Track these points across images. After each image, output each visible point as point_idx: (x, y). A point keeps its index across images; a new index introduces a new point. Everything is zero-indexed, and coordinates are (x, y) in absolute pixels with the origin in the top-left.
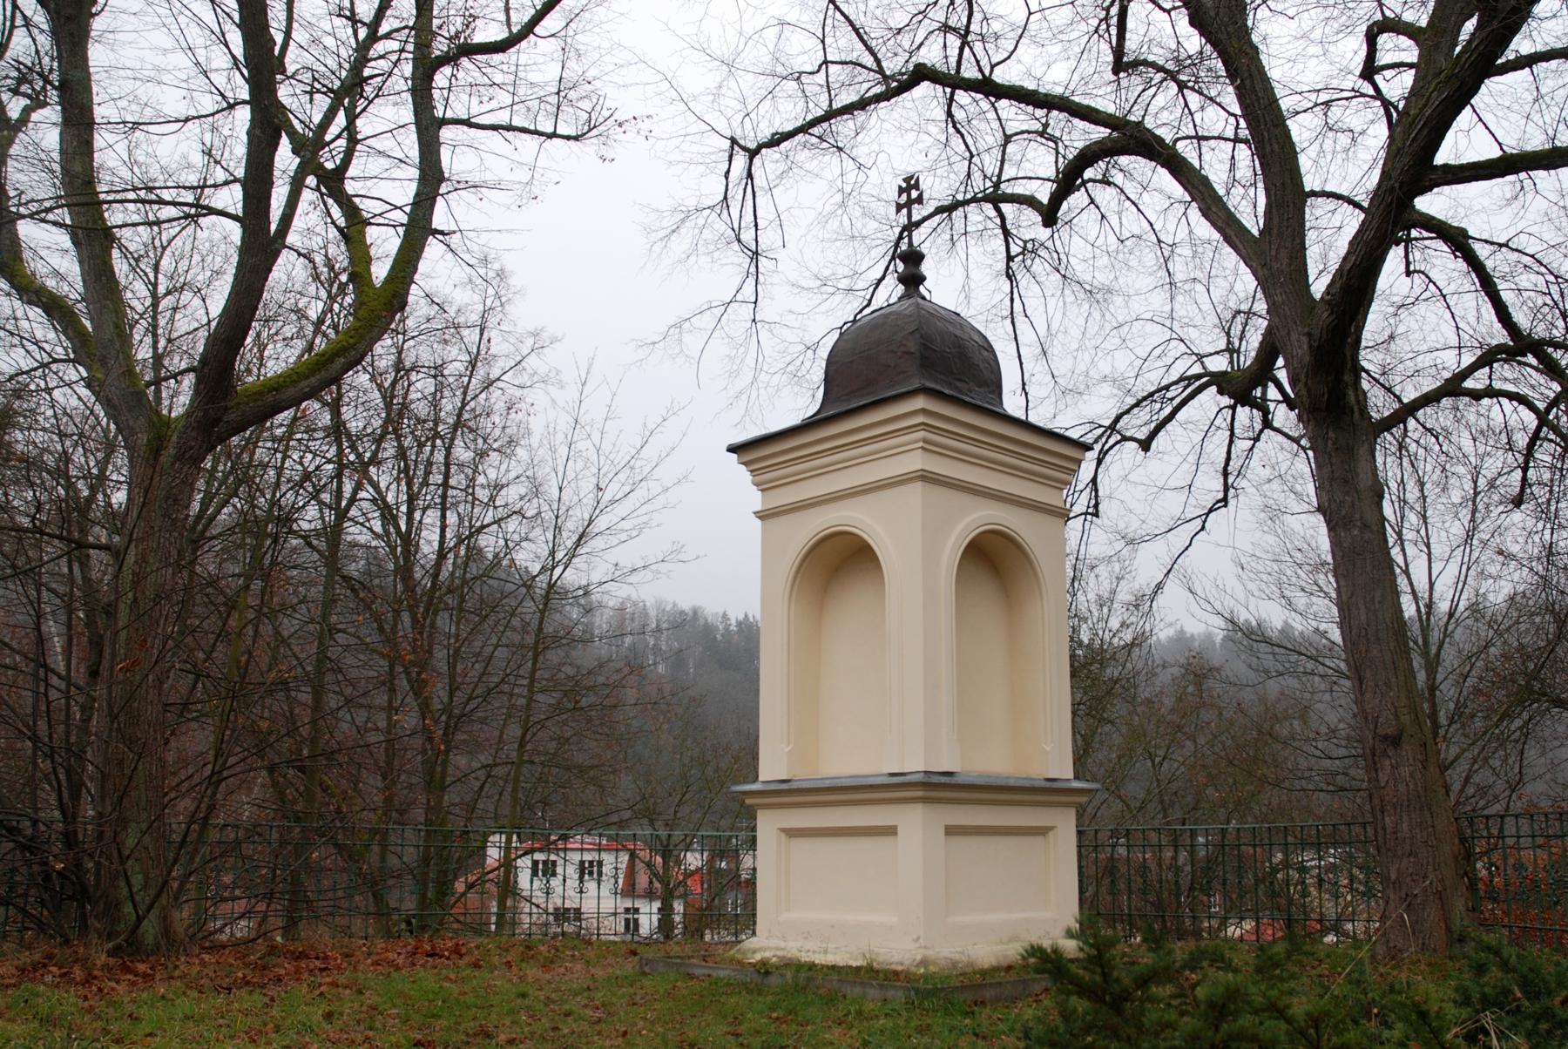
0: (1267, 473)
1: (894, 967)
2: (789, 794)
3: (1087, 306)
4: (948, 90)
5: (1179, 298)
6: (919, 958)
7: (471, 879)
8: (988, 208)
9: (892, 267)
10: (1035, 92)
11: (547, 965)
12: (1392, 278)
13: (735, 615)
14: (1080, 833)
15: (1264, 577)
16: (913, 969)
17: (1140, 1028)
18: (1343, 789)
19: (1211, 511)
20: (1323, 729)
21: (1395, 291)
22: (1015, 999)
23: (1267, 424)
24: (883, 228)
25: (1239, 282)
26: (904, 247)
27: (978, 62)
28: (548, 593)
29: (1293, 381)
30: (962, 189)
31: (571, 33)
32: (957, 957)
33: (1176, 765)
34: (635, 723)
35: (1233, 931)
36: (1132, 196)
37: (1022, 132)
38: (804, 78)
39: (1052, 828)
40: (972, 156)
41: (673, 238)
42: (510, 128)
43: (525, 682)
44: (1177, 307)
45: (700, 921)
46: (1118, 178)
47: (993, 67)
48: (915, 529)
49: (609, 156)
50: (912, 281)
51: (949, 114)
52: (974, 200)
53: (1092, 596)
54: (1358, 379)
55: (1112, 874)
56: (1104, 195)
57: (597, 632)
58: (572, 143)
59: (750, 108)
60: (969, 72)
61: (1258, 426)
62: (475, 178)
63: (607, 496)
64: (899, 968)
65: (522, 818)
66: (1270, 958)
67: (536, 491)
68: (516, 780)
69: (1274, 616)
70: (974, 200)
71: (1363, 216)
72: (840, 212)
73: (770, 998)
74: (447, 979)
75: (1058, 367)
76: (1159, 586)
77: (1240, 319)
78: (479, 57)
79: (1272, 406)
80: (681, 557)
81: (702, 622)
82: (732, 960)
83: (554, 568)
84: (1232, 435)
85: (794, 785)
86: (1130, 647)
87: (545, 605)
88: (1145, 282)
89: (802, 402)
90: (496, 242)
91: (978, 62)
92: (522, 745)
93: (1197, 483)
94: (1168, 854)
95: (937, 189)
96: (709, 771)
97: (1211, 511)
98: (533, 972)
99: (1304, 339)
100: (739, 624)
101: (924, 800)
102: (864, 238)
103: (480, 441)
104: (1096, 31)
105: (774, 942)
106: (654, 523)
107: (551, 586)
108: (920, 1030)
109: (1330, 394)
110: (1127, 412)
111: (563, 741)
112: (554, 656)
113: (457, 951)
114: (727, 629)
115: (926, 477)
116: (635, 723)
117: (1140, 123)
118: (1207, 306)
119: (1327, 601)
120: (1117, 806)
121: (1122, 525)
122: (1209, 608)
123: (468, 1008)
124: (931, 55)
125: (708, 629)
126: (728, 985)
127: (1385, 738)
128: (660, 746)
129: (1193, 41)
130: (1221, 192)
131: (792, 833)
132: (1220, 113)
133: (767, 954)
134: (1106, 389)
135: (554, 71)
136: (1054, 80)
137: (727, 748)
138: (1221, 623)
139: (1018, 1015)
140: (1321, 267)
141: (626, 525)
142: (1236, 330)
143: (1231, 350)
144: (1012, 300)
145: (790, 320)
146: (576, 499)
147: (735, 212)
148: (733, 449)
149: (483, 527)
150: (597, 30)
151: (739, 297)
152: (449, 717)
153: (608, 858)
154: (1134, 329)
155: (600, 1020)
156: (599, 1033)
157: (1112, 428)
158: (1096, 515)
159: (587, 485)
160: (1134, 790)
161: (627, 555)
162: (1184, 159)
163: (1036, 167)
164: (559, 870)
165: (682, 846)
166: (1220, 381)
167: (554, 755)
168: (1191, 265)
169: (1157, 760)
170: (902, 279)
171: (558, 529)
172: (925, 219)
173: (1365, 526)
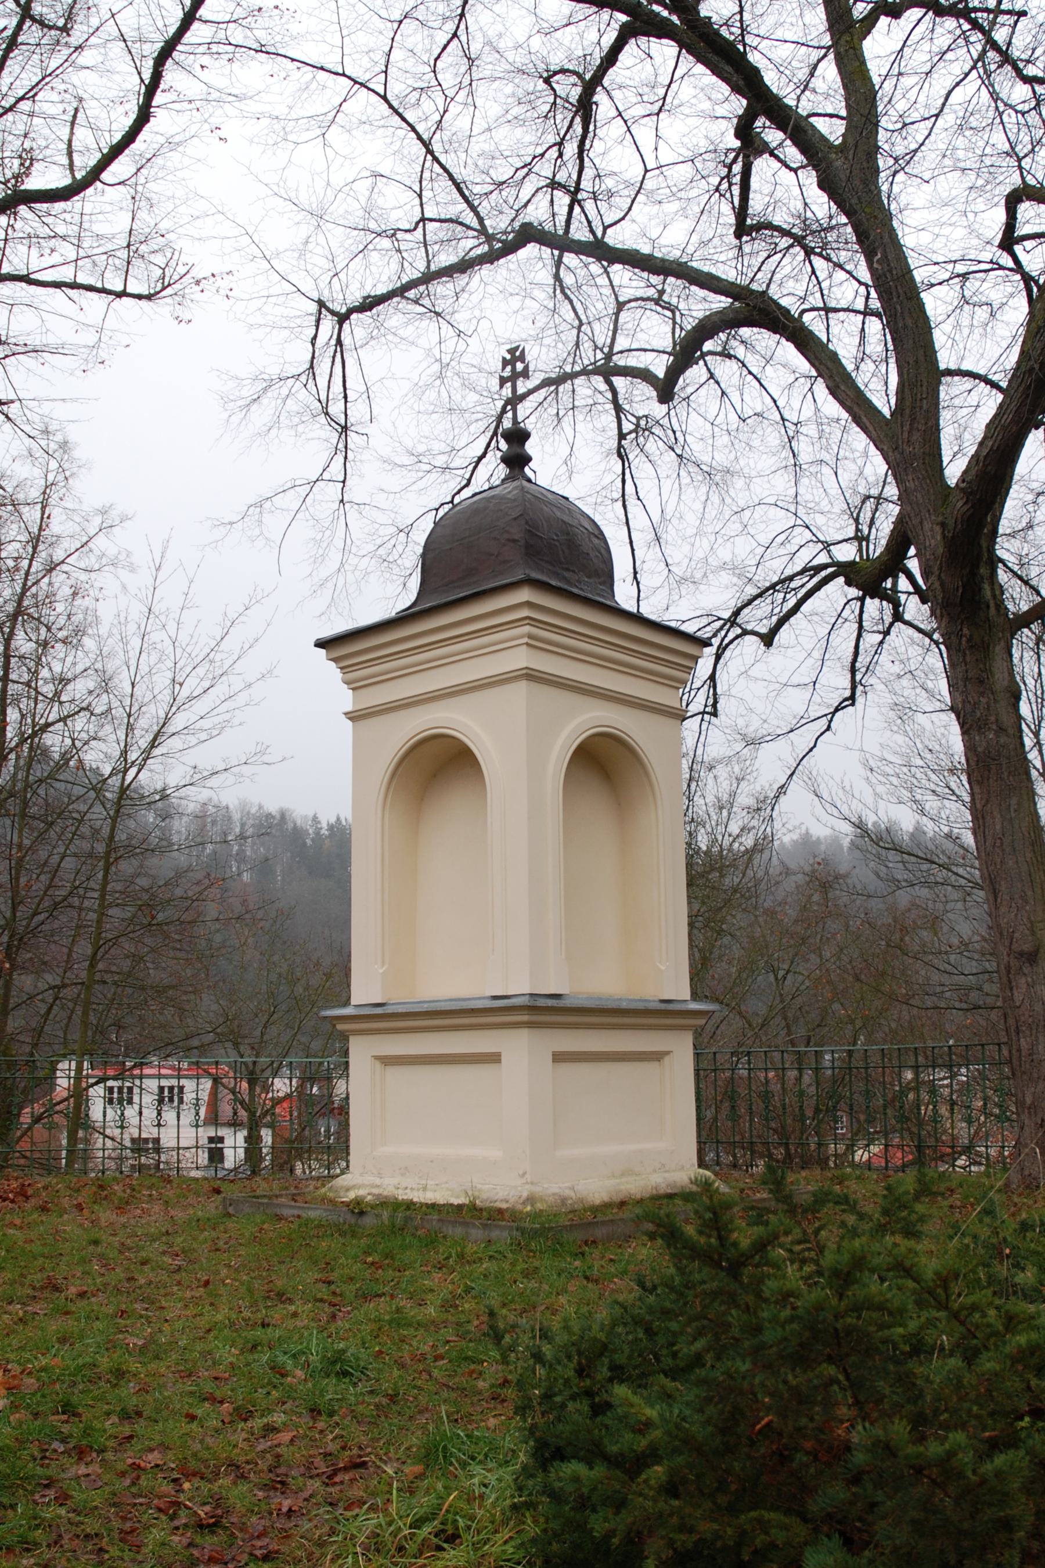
0: (897, 668)
1: (498, 1205)
2: (383, 1019)
3: (704, 489)
4: (556, 252)
5: (804, 481)
6: (525, 1194)
7: (38, 1109)
8: (599, 381)
9: (493, 444)
10: (650, 257)
11: (121, 1208)
12: (1032, 462)
13: (327, 818)
14: (697, 1055)
15: (895, 780)
16: (519, 1207)
17: (759, 1295)
18: (977, 1007)
19: (837, 710)
20: (955, 941)
21: (1034, 477)
22: (628, 1238)
23: (898, 617)
24: (484, 403)
25: (868, 465)
26: (507, 424)
27: (589, 222)
28: (120, 798)
29: (925, 575)
30: (570, 360)
31: (142, 180)
32: (568, 1193)
33: (801, 978)
34: (218, 938)
35: (860, 1155)
36: (754, 371)
37: (636, 300)
38: (400, 235)
39: (668, 1053)
40: (581, 324)
41: (254, 407)
42: (74, 286)
43: (96, 895)
44: (801, 490)
45: (290, 1150)
46: (740, 351)
47: (605, 228)
48: (517, 730)
49: (186, 317)
50: (517, 461)
51: (557, 277)
52: (584, 372)
53: (710, 799)
54: (994, 574)
55: (731, 1098)
56: (726, 370)
57: (175, 839)
58: (143, 303)
59: (339, 267)
60: (579, 233)
61: (888, 619)
62: (35, 341)
63: (185, 692)
64: (504, 1206)
65: (94, 1042)
66: (897, 1200)
67: (105, 685)
68: (87, 1003)
69: (905, 820)
70: (584, 372)
71: (1000, 397)
72: (438, 382)
73: (364, 1241)
74: (12, 1225)
75: (675, 554)
76: (782, 790)
77: (869, 505)
78: (37, 206)
79: (903, 598)
80: (266, 758)
81: (290, 826)
82: (323, 1199)
83: (126, 771)
84: (861, 627)
85: (389, 1010)
86: (751, 853)
87: (117, 811)
88: (767, 463)
89: (394, 590)
90: (60, 412)
91: (589, 222)
92: (92, 966)
93: (822, 680)
94: (792, 1074)
95: (543, 360)
96: (299, 990)
97: (837, 710)
98: (106, 1215)
99: (938, 529)
100: (331, 827)
101: (530, 1025)
102: (463, 411)
103: (43, 630)
104: (717, 190)
105: (369, 1179)
106: (236, 722)
107: (123, 790)
108: (526, 1274)
109: (964, 587)
110: (750, 602)
111: (138, 959)
112: (127, 867)
113: (23, 1193)
114: (317, 832)
115: (531, 676)
116: (218, 938)
117: (764, 293)
118: (834, 490)
119: (959, 805)
120: (738, 1023)
121: (741, 722)
122: (835, 812)
123: (35, 1258)
124: (538, 213)
125: (298, 833)
126: (320, 1226)
127: (1021, 954)
128: (241, 961)
129: (821, 205)
130: (850, 367)
131: (388, 1061)
132: (849, 284)
133: (361, 1192)
134: (725, 577)
135: (123, 222)
136: (671, 240)
137: (318, 964)
138: (846, 828)
139: (632, 1255)
140: (956, 449)
141: (205, 724)
142: (866, 516)
143: (860, 538)
144: (624, 481)
145: (381, 500)
146: (149, 696)
147: (322, 382)
148: (321, 644)
149: (48, 725)
150: (170, 177)
151: (326, 476)
152: (11, 937)
153: (189, 1085)
154: (756, 515)
155: (179, 1269)
156: (179, 1283)
157: (733, 621)
158: (715, 714)
159: (162, 680)
160: (757, 1007)
161: (206, 757)
162: (811, 332)
163: (650, 338)
164: (136, 1099)
165: (268, 1072)
166: (848, 571)
167: (129, 974)
168: (817, 446)
169: (781, 973)
170: (506, 460)
171: (130, 728)
172: (530, 392)
173: (1001, 729)
